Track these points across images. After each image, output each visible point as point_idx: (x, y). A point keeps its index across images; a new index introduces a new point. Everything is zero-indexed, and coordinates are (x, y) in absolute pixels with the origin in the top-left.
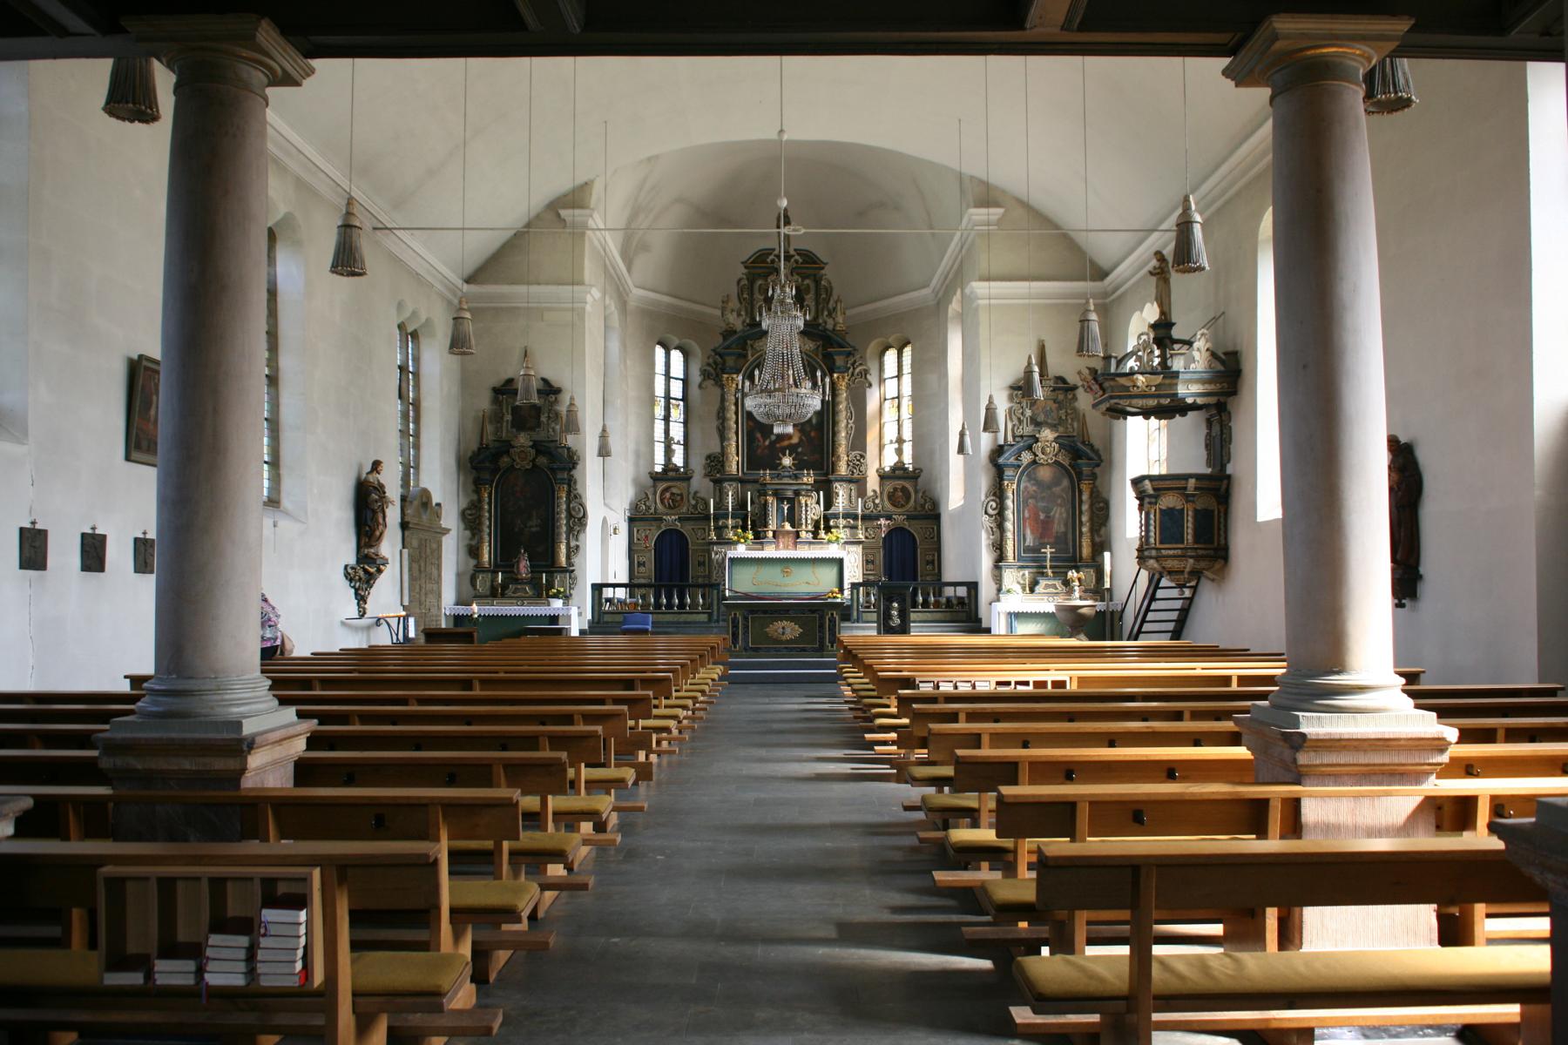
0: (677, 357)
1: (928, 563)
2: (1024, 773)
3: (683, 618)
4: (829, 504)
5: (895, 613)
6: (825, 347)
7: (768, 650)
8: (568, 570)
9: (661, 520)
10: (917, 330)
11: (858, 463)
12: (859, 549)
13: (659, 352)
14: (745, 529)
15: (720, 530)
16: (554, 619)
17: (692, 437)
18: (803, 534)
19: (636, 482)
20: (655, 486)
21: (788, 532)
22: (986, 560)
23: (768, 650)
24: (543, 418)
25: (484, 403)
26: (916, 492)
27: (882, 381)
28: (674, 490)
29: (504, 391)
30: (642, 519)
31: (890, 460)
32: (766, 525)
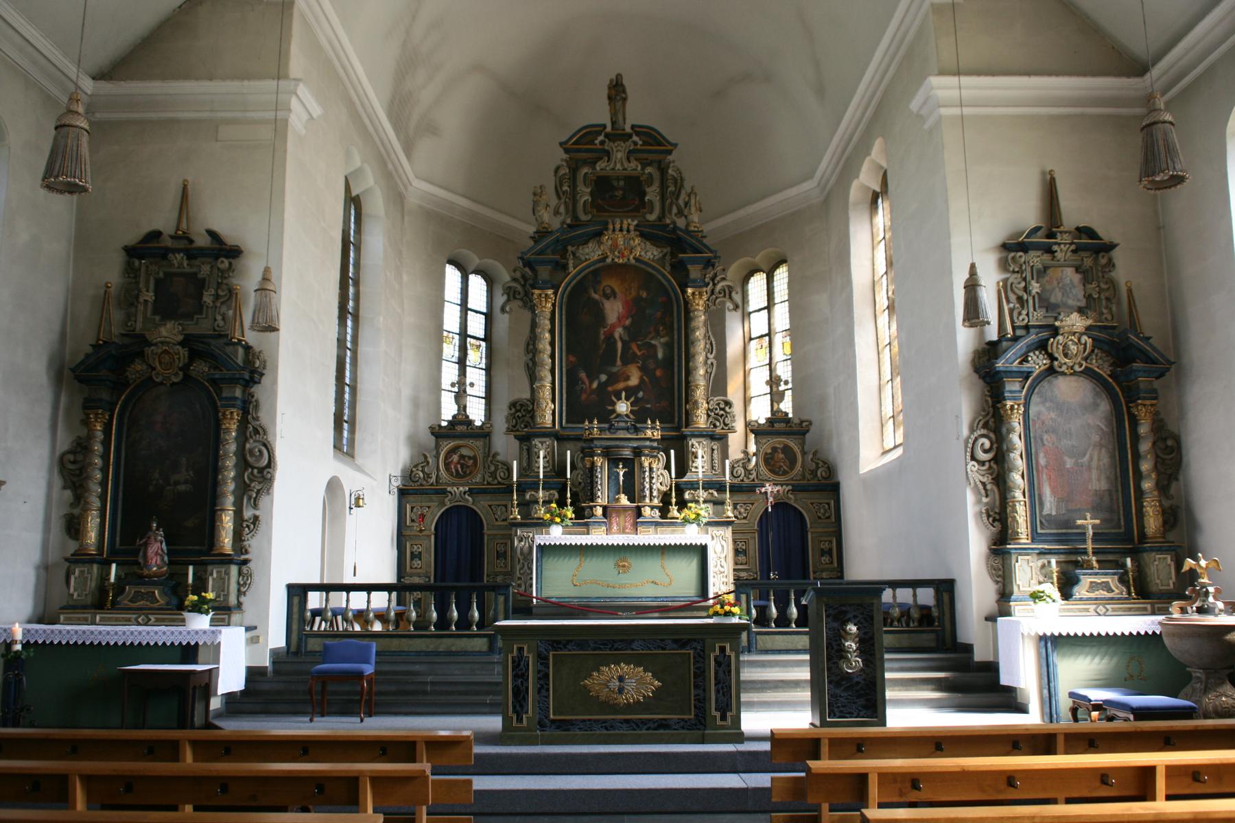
0: (477, 285)
1: (823, 553)
2: (825, 749)
3: (444, 645)
4: (682, 469)
5: (851, 645)
6: (673, 255)
7: (588, 725)
10: (802, 243)
11: (721, 413)
12: (728, 533)
13: (452, 276)
14: (562, 504)
16: (189, 652)
17: (495, 386)
18: (647, 511)
19: (412, 440)
20: (437, 447)
21: (625, 508)
22: (976, 542)
23: (588, 725)
24: (207, 298)
25: (112, 273)
26: (804, 453)
27: (746, 315)
28: (465, 452)
29: (145, 251)
30: (417, 492)
31: (760, 411)
32: (593, 498)
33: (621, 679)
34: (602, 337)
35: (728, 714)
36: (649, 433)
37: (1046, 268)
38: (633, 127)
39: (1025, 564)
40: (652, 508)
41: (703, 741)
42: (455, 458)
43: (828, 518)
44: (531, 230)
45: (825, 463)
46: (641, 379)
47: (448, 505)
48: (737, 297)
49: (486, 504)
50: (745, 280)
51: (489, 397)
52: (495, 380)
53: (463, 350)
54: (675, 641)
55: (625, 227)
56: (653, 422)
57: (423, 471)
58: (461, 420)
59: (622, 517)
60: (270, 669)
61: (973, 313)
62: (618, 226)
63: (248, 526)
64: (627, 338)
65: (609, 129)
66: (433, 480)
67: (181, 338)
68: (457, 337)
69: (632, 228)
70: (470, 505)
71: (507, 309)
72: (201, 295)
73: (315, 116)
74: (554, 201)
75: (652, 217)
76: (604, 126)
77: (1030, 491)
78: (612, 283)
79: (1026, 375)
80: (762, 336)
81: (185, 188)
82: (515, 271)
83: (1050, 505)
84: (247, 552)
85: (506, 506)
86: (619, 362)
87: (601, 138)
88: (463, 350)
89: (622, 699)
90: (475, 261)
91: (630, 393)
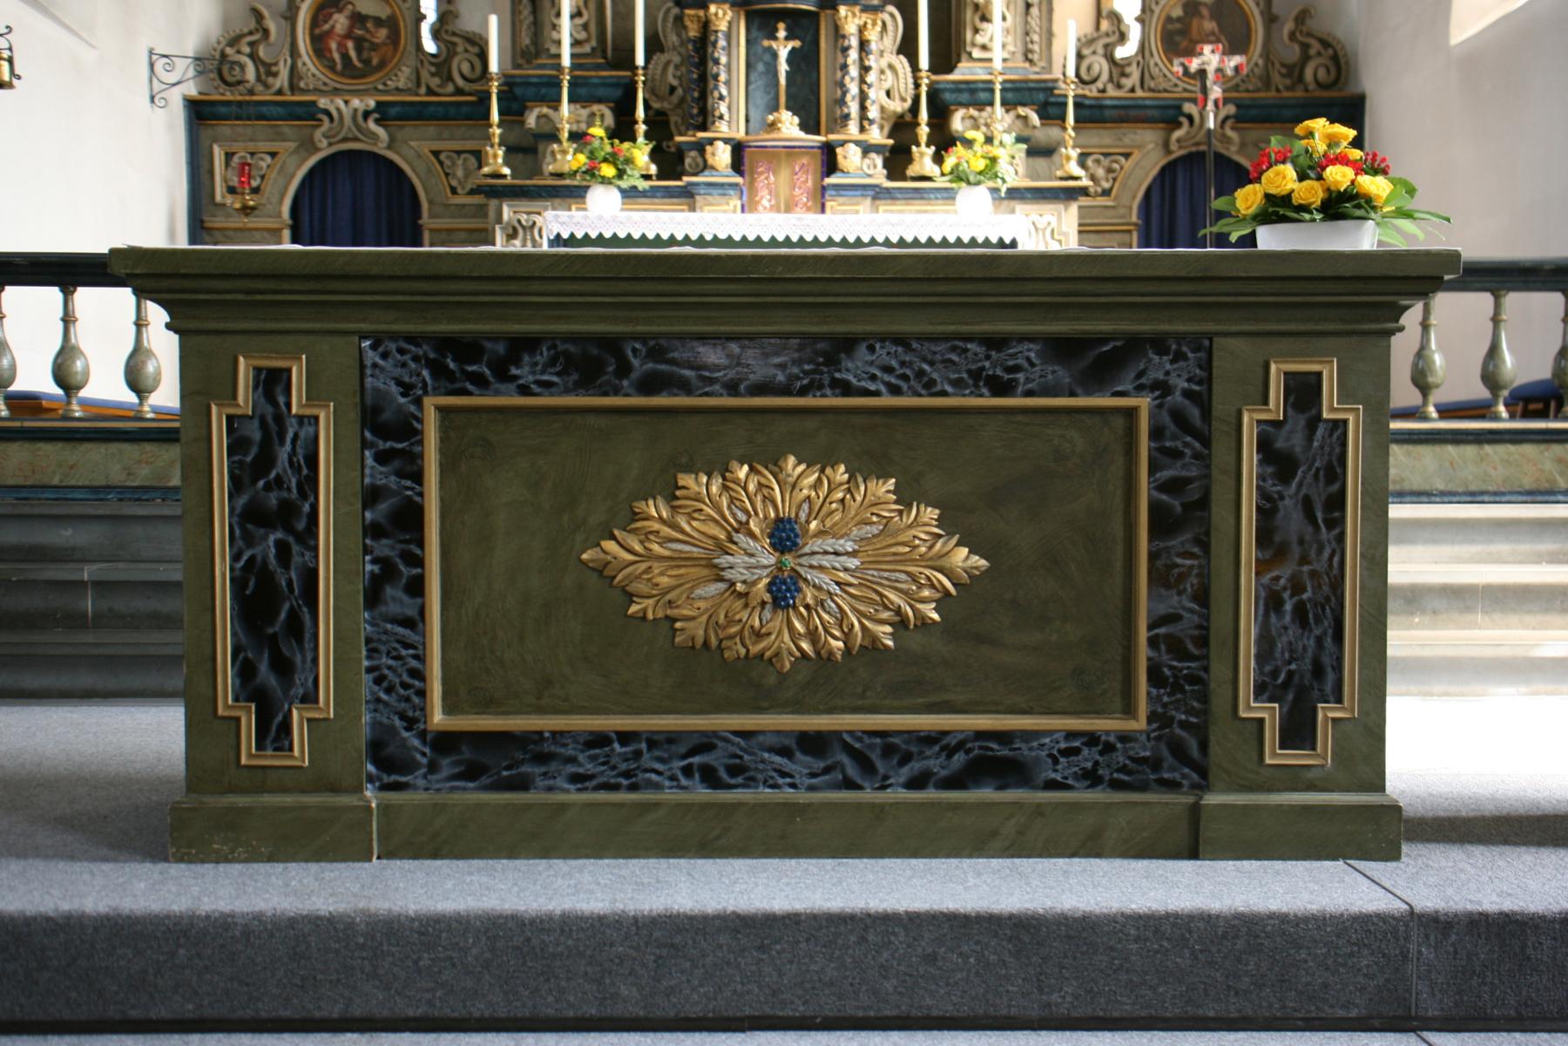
4: (947, 52)
7: (620, 760)
9: (309, 113)
14: (623, 131)
15: (528, 148)
18: (850, 157)
21: (792, 151)
23: (620, 760)
32: (704, 119)
33: (784, 536)
35: (1326, 713)
40: (867, 149)
41: (1191, 843)
42: (340, 22)
45: (1325, 44)
49: (425, 147)
54: (1062, 348)
57: (253, 56)
59: (784, 174)
70: (381, 149)
89: (786, 638)
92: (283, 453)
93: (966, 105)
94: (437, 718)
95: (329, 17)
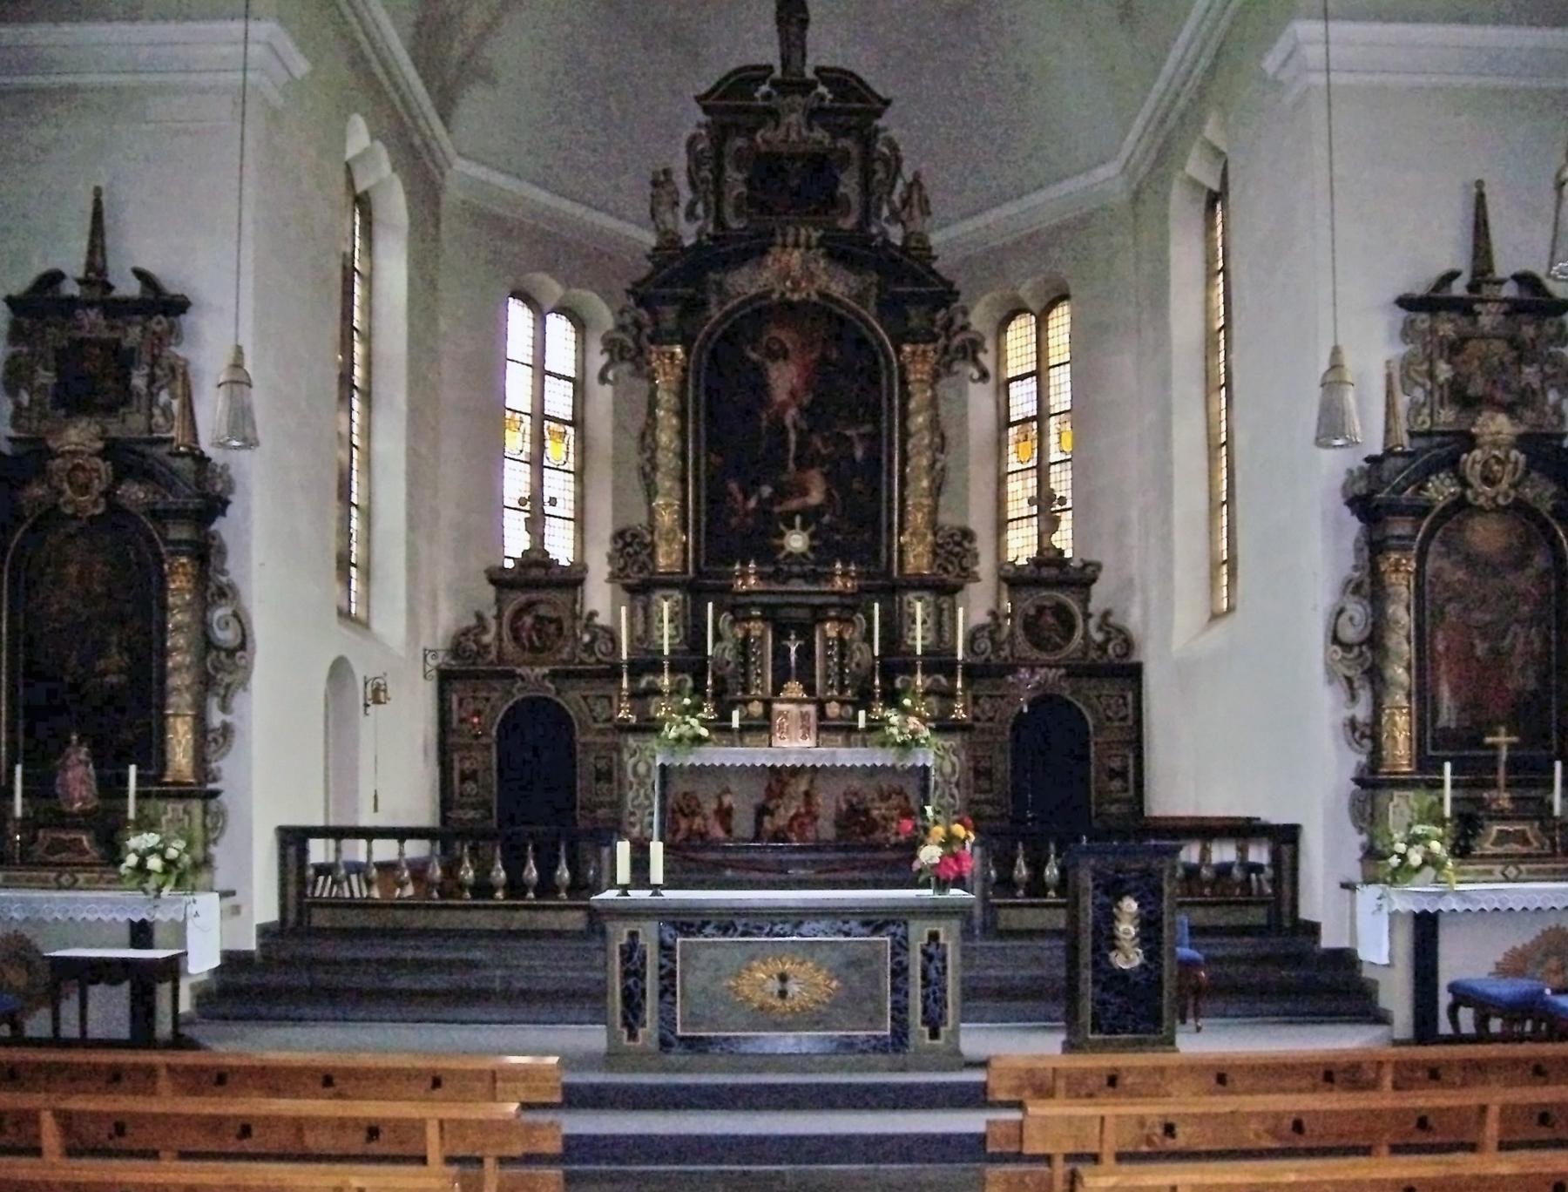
0: (559, 329)
1: (1114, 774)
3: (520, 920)
8: (201, 791)
13: (519, 317)
14: (698, 690)
20: (498, 601)
24: (139, 381)
28: (543, 610)
31: (1021, 545)
33: (783, 978)
34: (764, 423)
35: (942, 1030)
36: (839, 583)
37: (1464, 340)
38: (818, 71)
39: (1402, 802)
42: (528, 620)
43: (1124, 719)
44: (650, 239)
46: (828, 493)
47: (519, 697)
48: (987, 360)
50: (1003, 326)
51: (580, 520)
52: (589, 492)
53: (539, 441)
55: (802, 239)
56: (846, 563)
58: (536, 559)
60: (257, 954)
61: (1331, 427)
62: (790, 239)
63: (215, 740)
64: (804, 425)
65: (778, 73)
66: (493, 656)
67: (99, 445)
68: (527, 419)
69: (814, 242)
70: (551, 695)
71: (610, 375)
72: (127, 377)
73: (298, 75)
74: (686, 195)
75: (848, 223)
76: (770, 68)
77: (1419, 692)
78: (787, 337)
79: (1425, 510)
80: (1026, 421)
81: (98, 203)
82: (622, 312)
83: (1448, 714)
84: (215, 780)
85: (610, 699)
86: (791, 465)
87: (765, 88)
88: (539, 441)
90: (553, 290)
91: (810, 517)
92: (636, 955)
93: (903, 673)
94: (679, 1033)
95: (520, 618)
